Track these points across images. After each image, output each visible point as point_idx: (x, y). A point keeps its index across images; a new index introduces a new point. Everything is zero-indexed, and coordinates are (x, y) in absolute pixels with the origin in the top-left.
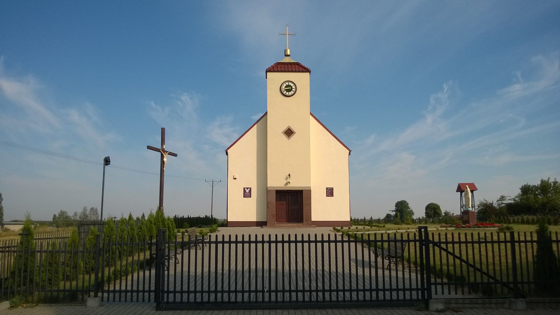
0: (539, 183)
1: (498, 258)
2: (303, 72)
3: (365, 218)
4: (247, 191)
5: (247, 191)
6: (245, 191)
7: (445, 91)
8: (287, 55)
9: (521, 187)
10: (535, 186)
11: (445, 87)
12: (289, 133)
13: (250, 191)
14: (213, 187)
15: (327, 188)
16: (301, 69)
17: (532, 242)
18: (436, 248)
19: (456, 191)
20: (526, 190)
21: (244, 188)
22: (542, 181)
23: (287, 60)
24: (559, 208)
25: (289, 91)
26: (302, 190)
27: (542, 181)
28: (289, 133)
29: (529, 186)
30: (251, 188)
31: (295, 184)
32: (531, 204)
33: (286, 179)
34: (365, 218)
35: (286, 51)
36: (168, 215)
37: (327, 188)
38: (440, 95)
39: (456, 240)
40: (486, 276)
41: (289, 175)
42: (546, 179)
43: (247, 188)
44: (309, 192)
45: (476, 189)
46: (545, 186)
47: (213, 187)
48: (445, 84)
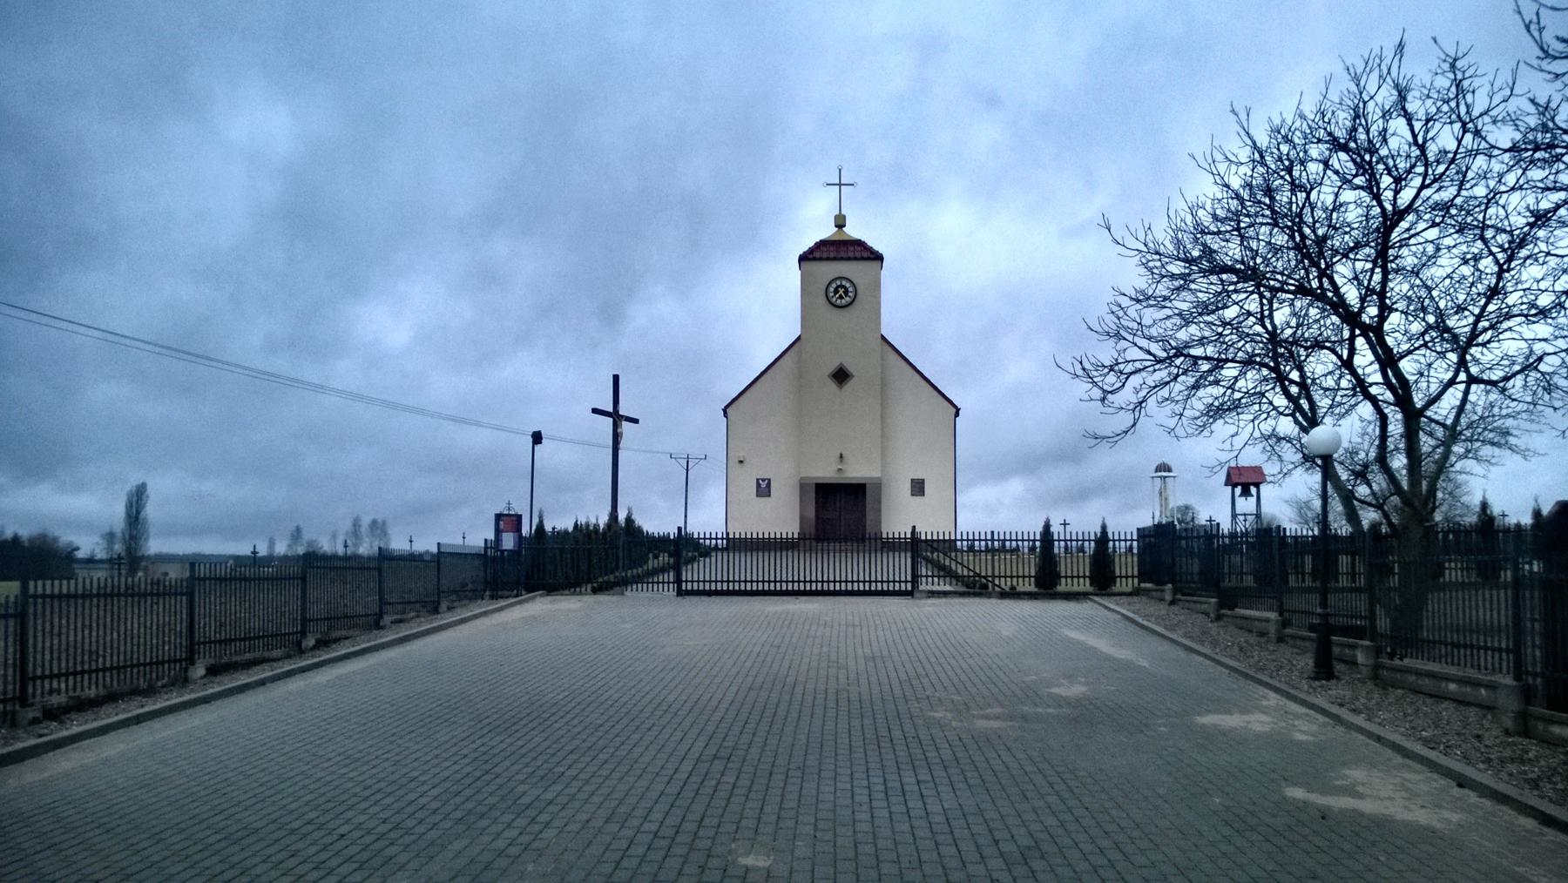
1: (1447, 703)
2: (868, 259)
3: (1104, 528)
4: (763, 485)
5: (763, 485)
6: (758, 485)
13: (769, 485)
14: (687, 470)
15: (912, 480)
16: (865, 254)
17: (1030, 577)
18: (978, 571)
21: (758, 480)
25: (846, 292)
26: (864, 485)
28: (841, 376)
30: (769, 480)
34: (1104, 528)
37: (912, 480)
39: (1021, 579)
40: (1473, 790)
43: (763, 480)
47: (687, 470)
48: (740, 859)
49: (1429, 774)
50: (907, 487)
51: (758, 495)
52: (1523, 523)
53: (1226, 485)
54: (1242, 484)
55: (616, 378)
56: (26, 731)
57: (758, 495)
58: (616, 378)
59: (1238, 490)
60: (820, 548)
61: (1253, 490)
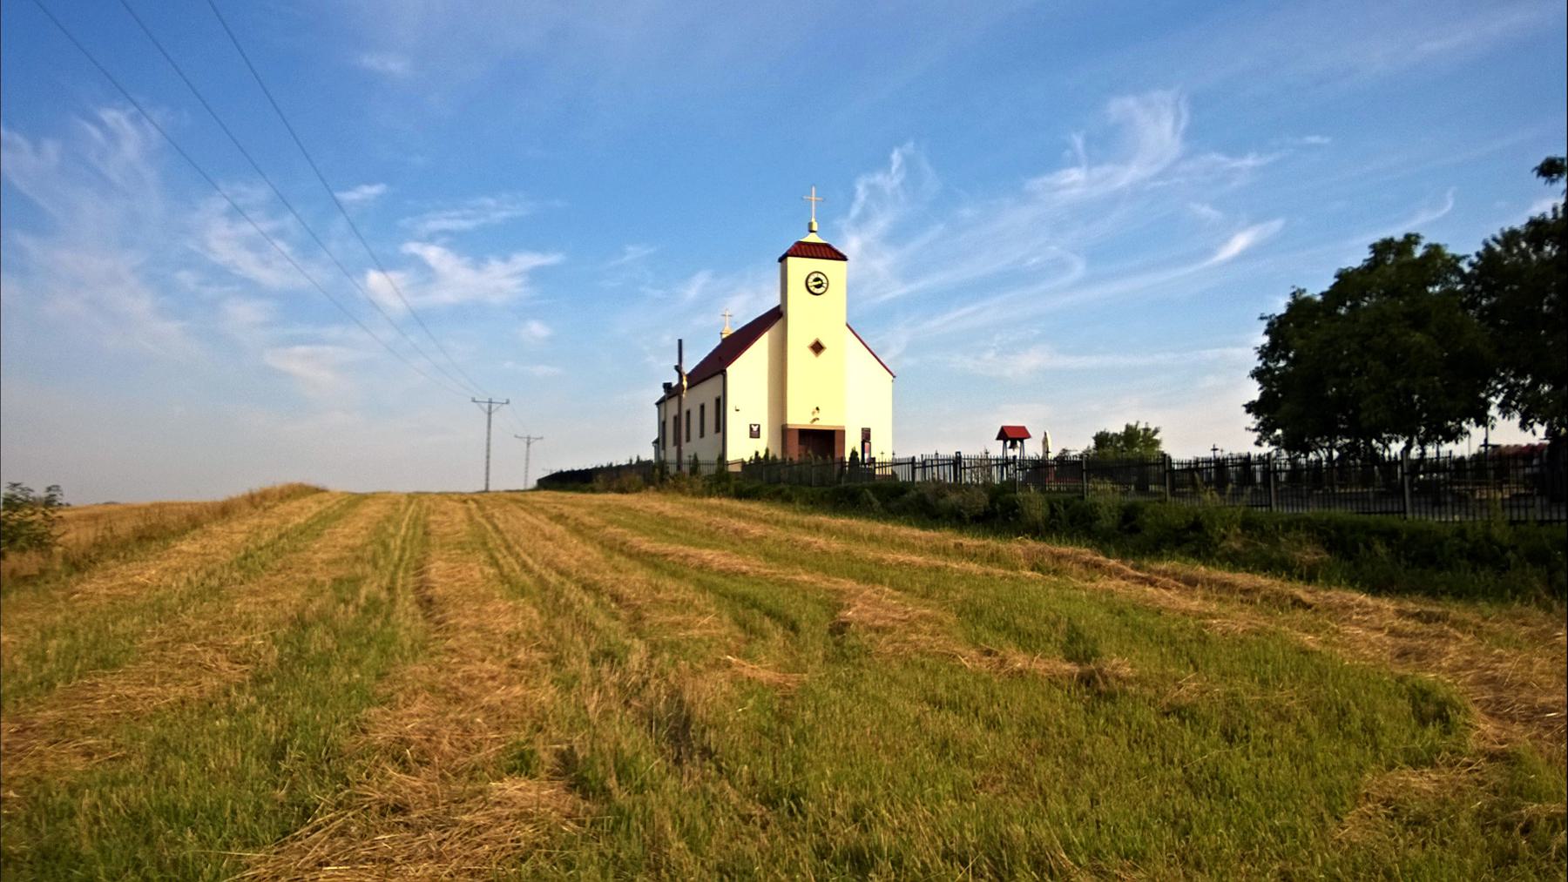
0: (1123, 430)
4: (755, 429)
5: (755, 429)
6: (751, 429)
7: (894, 168)
8: (812, 231)
9: (1094, 435)
10: (1115, 435)
11: (896, 157)
12: (817, 348)
13: (759, 429)
14: (490, 414)
19: (996, 436)
20: (1102, 439)
22: (1128, 427)
23: (812, 238)
24: (898, 863)
25: (818, 286)
27: (1128, 427)
28: (817, 348)
29: (1108, 434)
31: (826, 422)
32: (189, 853)
33: (813, 413)
35: (810, 224)
36: (638, 458)
38: (879, 178)
41: (817, 409)
42: (1133, 423)
44: (843, 432)
45: (1029, 436)
46: (1131, 435)
47: (490, 414)
49: (598, 577)
50: (764, 432)
51: (751, 437)
52: (643, 458)
53: (998, 438)
54: (1011, 439)
55: (680, 341)
56: (115, 557)
57: (751, 437)
58: (680, 341)
59: (1009, 443)
60: (1295, 503)
61: (1019, 443)
